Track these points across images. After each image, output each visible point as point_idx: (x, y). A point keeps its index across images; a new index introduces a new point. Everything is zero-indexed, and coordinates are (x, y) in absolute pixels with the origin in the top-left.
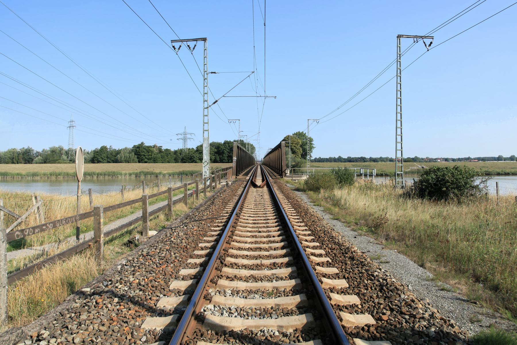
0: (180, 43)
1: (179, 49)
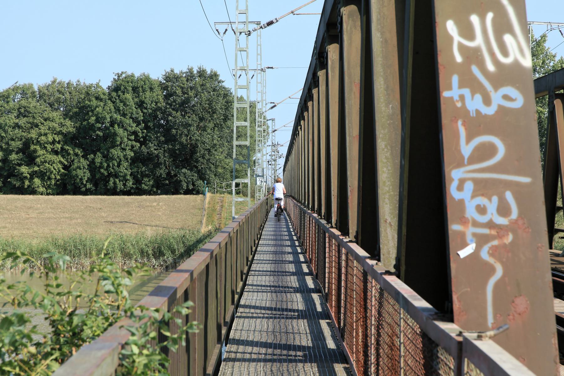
1: (225, 33)
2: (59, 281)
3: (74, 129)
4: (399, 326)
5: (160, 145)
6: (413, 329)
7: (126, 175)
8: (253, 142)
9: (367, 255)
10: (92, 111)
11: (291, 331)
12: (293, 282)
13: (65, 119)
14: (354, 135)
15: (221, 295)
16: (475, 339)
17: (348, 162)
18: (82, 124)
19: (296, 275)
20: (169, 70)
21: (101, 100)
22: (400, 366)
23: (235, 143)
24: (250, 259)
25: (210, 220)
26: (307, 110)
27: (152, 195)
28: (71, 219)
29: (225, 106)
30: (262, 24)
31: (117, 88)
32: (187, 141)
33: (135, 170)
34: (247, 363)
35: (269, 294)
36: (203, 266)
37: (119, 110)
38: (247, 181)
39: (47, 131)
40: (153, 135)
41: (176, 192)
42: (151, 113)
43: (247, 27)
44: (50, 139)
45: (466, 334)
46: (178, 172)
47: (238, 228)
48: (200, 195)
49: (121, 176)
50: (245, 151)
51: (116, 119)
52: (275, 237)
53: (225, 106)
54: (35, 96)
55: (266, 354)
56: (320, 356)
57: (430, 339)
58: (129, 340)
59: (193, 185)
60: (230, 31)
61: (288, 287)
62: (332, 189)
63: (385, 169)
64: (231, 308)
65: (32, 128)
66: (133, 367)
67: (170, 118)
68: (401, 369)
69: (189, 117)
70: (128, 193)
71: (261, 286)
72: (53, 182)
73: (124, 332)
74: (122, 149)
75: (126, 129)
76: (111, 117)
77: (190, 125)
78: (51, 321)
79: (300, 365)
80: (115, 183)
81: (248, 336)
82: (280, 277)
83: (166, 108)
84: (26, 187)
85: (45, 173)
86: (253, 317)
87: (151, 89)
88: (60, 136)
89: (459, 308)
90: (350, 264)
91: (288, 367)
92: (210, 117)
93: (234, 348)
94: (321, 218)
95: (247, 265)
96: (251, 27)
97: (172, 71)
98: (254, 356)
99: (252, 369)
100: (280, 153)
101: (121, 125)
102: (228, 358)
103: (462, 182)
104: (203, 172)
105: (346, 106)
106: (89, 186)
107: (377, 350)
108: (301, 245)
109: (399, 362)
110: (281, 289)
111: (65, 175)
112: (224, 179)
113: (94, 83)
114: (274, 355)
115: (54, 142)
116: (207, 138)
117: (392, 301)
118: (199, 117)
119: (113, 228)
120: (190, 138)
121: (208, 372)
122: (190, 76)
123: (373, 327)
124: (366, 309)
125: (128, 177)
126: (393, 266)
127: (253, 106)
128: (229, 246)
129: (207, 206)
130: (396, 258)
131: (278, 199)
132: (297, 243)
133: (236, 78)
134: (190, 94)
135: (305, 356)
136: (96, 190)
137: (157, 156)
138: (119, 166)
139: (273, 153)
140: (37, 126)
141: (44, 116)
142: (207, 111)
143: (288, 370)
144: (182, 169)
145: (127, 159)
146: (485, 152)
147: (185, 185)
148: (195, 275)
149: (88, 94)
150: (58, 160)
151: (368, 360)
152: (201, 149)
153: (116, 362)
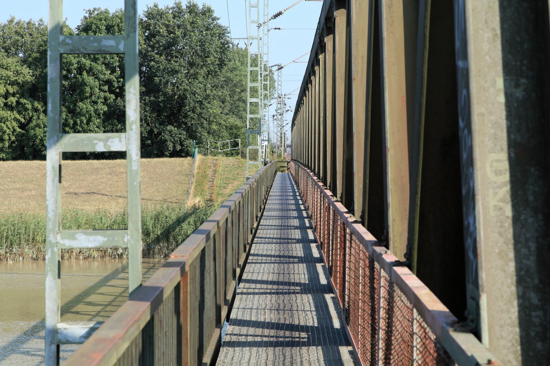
20: (151, 5)
28: (23, 190)
29: (221, 48)
41: (161, 155)
48: (189, 158)
51: (85, 65)
52: (280, 198)
72: (7, 144)
74: (93, 102)
75: (96, 78)
77: (177, 72)
88: (15, 87)
97: (156, 6)
101: (90, 71)
104: (194, 129)
112: (219, 137)
116: (197, 86)
122: (178, 12)
129: (196, 171)
134: (177, 33)
138: (88, 123)
144: (167, 125)
145: (99, 115)
147: (171, 146)
150: (13, 117)
152: (190, 102)
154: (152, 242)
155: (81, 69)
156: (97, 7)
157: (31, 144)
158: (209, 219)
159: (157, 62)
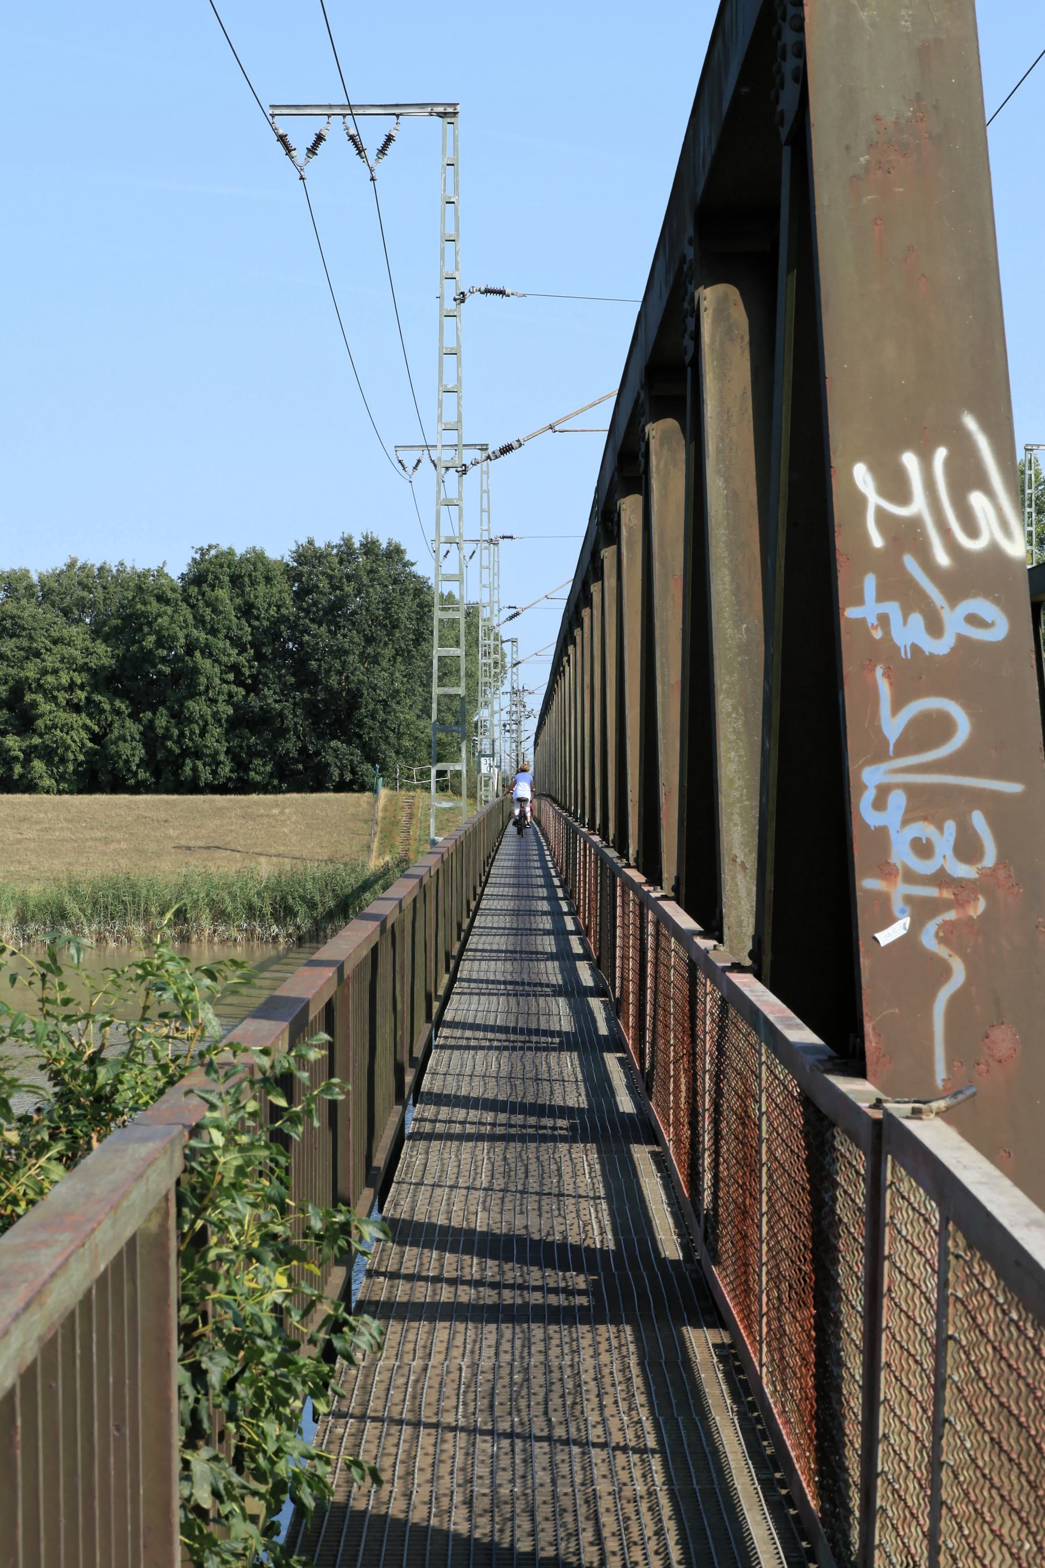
0: (318, 124)
1: (415, 468)
2: (67, 993)
3: (113, 661)
4: (759, 1077)
5: (285, 691)
6: (786, 1087)
7: (217, 753)
8: (472, 689)
9: (696, 927)
10: (150, 624)
11: (546, 1076)
12: (552, 972)
13: (94, 640)
14: (673, 682)
15: (403, 1006)
16: (907, 1118)
17: (660, 735)
18: (128, 650)
19: (557, 959)
20: (303, 541)
21: (167, 602)
22: (760, 1160)
23: (436, 691)
24: (465, 926)
25: (387, 844)
26: (581, 625)
27: (270, 793)
28: (106, 841)
29: (418, 613)
30: (490, 451)
31: (201, 576)
32: (340, 684)
33: (235, 742)
34: (456, 1143)
35: (502, 999)
36: (366, 951)
37: (203, 622)
38: (461, 766)
39: (58, 665)
40: (273, 672)
41: (319, 787)
42: (269, 628)
43: (461, 457)
44: (65, 679)
45: (890, 1106)
46: (323, 747)
47: (440, 865)
48: (367, 794)
49: (208, 756)
50: (456, 705)
51: (197, 639)
52: (516, 881)
53: (418, 613)
54: (32, 595)
55: (493, 1125)
56: (604, 1129)
57: (818, 1111)
58: (204, 1117)
59: (353, 772)
60: (426, 463)
61: (541, 985)
62: (629, 788)
63: (733, 754)
64: (424, 1029)
65: (27, 658)
66: (213, 1173)
67: (306, 638)
68: (762, 1165)
69: (345, 636)
70: (222, 789)
71: (487, 982)
72: (71, 767)
73: (194, 1100)
74: (210, 700)
75: (216, 661)
76: (187, 636)
77: (346, 653)
78: (52, 1071)
79: (563, 1147)
80: (194, 769)
81: (459, 1087)
82: (526, 963)
83: (298, 617)
84: (16, 777)
85: (54, 751)
86: (468, 1048)
87: (268, 580)
88: (84, 674)
89: (878, 1049)
90: (663, 944)
91: (538, 1151)
92: (388, 635)
93: (430, 1111)
94: (608, 847)
95: (459, 939)
96: (469, 456)
97: (311, 542)
98: (470, 1129)
99: (465, 1156)
100: (528, 709)
101: (207, 651)
102: (418, 1133)
103: (883, 792)
104: (374, 746)
105: (657, 623)
106: (142, 775)
107: (716, 1122)
108: (569, 897)
109: (759, 1152)
110: (527, 988)
111: (95, 753)
112: (414, 760)
113: (154, 567)
114: (511, 1126)
115: (71, 687)
116: (380, 678)
117: (744, 1027)
118: (364, 635)
119: (193, 861)
120: (347, 677)
121: (375, 1164)
122: (346, 553)
123: (707, 1077)
124: (693, 1037)
125: (222, 757)
126: (746, 954)
127: (472, 613)
128: (420, 905)
129: (380, 814)
130: (754, 937)
131: (522, 801)
132: (560, 893)
133: (438, 557)
134: (346, 589)
135: (572, 1128)
136: (156, 783)
137: (281, 715)
138: (202, 735)
139: (514, 708)
140: (37, 654)
141: (53, 634)
142: (380, 624)
143: (538, 1158)
144: (330, 740)
145: (219, 721)
146: (930, 730)
147: (336, 773)
148: (348, 971)
149: (140, 589)
150: (80, 723)
151: (699, 1142)
152: (368, 704)
153: (179, 1163)
154: (323, 918)
155: (190, 648)
156: (214, 543)
157: (110, 767)
158: (367, 910)
159: (314, 636)
